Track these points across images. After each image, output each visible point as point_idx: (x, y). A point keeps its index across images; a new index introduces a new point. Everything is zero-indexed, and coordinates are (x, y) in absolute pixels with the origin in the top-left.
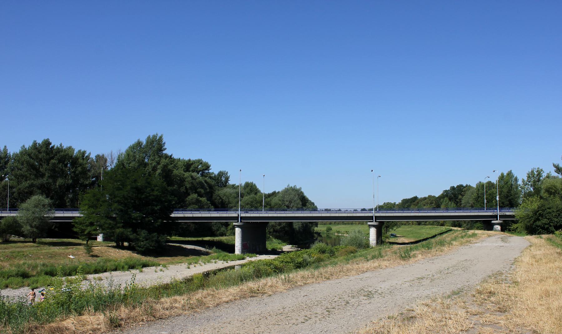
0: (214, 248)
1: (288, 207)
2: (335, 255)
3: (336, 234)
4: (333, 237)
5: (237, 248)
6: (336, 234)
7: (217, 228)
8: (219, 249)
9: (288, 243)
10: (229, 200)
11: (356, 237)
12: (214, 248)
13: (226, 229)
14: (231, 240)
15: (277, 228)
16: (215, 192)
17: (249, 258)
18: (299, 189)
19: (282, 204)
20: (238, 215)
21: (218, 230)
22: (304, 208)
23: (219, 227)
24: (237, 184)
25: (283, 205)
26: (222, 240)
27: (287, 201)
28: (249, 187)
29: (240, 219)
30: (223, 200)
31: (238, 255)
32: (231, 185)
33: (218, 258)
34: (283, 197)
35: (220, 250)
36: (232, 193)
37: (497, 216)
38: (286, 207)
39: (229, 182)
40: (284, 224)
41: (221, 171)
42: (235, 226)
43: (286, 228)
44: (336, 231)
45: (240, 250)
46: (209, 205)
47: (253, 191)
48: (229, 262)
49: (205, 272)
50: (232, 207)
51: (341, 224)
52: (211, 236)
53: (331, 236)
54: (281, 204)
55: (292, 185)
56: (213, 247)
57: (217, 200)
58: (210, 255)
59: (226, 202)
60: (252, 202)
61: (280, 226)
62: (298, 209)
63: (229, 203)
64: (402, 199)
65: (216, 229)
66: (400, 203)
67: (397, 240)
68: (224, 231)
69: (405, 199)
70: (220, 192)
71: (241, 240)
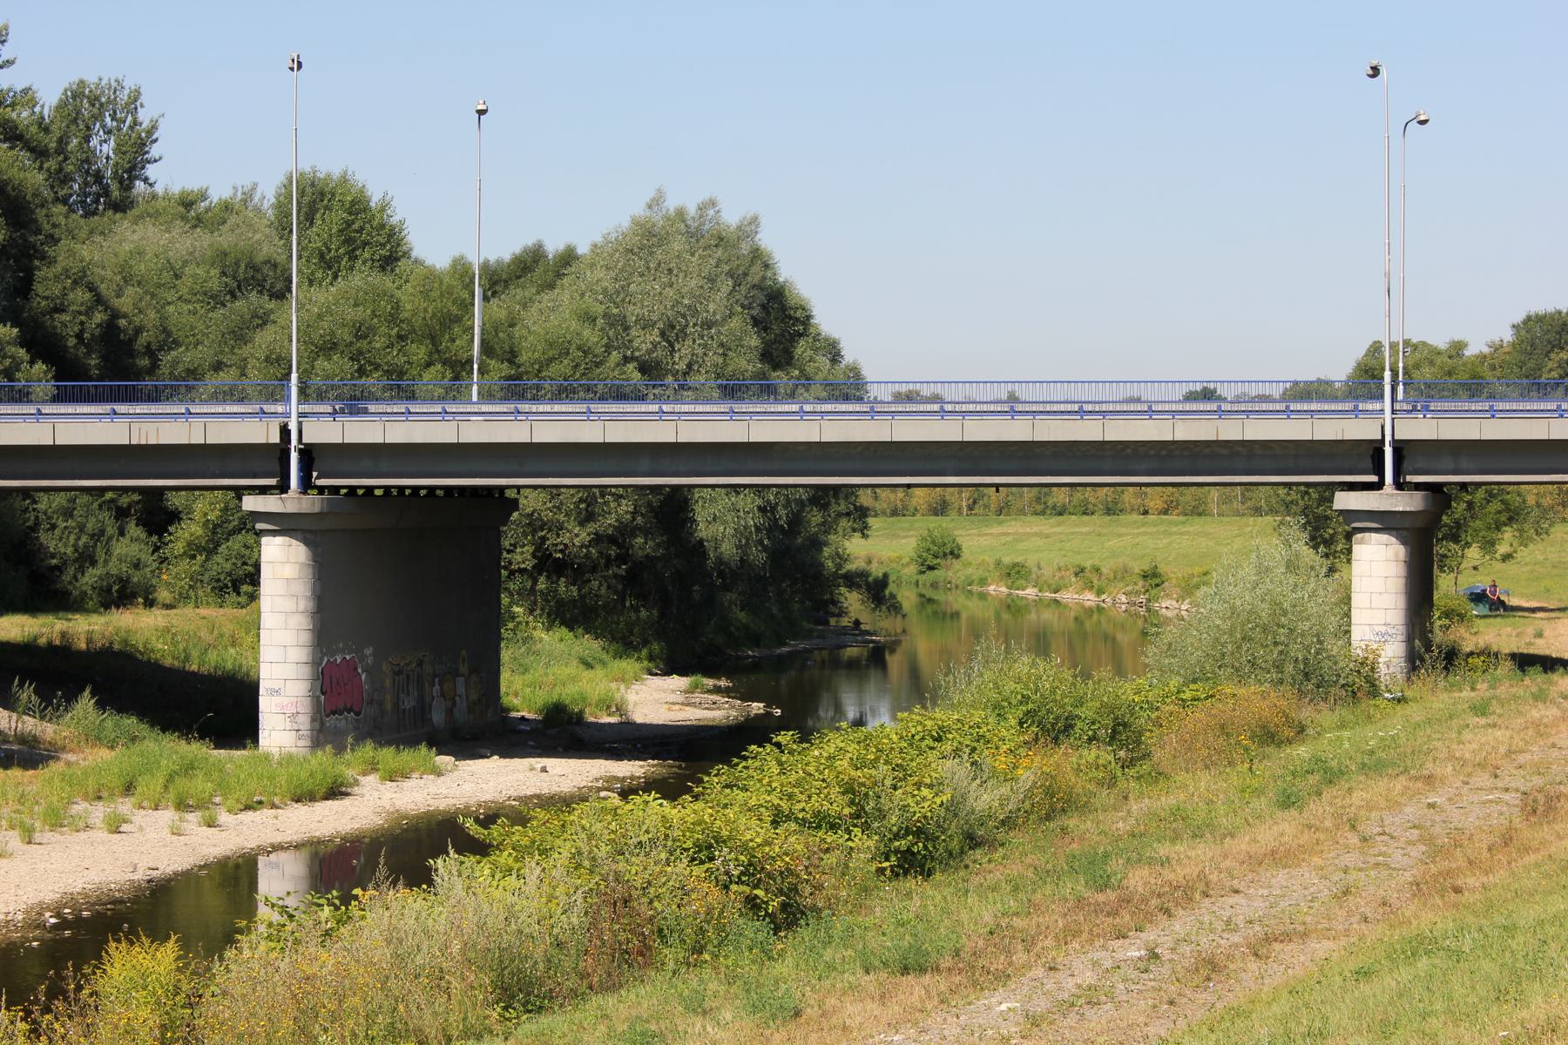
0: (85, 704)
1: (649, 369)
2: (1147, 756)
3: (997, 589)
4: (969, 607)
5: (276, 700)
6: (997, 589)
7: (84, 539)
8: (122, 709)
9: (651, 658)
10: (163, 318)
11: (1278, 609)
12: (85, 704)
13: (156, 549)
14: (203, 634)
15: (565, 538)
16: (50, 251)
17: (383, 779)
18: (739, 228)
19: (608, 348)
20: (285, 432)
21: (86, 558)
22: (780, 378)
23: (98, 535)
24: (219, 192)
25: (615, 356)
26: (138, 641)
27: (647, 325)
28: (338, 216)
29: (301, 461)
30: (115, 315)
31: (288, 760)
32: (167, 197)
33: (129, 789)
34: (619, 295)
35: (130, 722)
36: (185, 263)
37: (282, 451)
38: (637, 375)
39: (151, 171)
40: (626, 507)
41: (82, 83)
42: (260, 526)
43: (640, 540)
44: (998, 563)
45: (304, 722)
46: (12, 357)
47: (365, 244)
48: (224, 817)
49: (42, 908)
50: (193, 373)
51: (1022, 512)
52: (31, 606)
53: (956, 601)
54: (600, 350)
55: (684, 197)
56: (71, 697)
57: (66, 317)
58: (55, 767)
59: (138, 331)
60: (362, 332)
61: (592, 527)
62: (732, 391)
63: (168, 340)
64: (1519, 318)
65: (69, 550)
66: (1497, 348)
67: (1540, 635)
68: (137, 566)
69: (1552, 316)
70: (85, 252)
71: (306, 637)
